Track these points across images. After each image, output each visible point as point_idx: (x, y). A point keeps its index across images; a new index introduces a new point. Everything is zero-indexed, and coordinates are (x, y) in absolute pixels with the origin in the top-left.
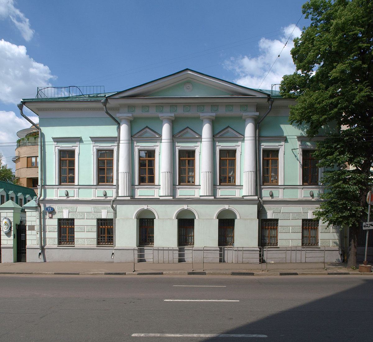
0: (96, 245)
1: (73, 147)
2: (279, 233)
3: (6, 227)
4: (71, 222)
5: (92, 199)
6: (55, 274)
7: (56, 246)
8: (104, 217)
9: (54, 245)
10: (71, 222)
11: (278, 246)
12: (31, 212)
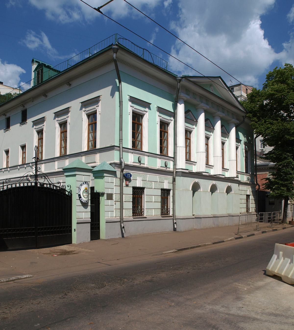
0: (160, 216)
1: (170, 120)
2: (125, 202)
3: (86, 195)
4: (142, 189)
5: (158, 169)
6: (214, 243)
7: (131, 218)
8: (138, 185)
9: (130, 216)
10: (142, 189)
11: (145, 216)
12: (110, 177)
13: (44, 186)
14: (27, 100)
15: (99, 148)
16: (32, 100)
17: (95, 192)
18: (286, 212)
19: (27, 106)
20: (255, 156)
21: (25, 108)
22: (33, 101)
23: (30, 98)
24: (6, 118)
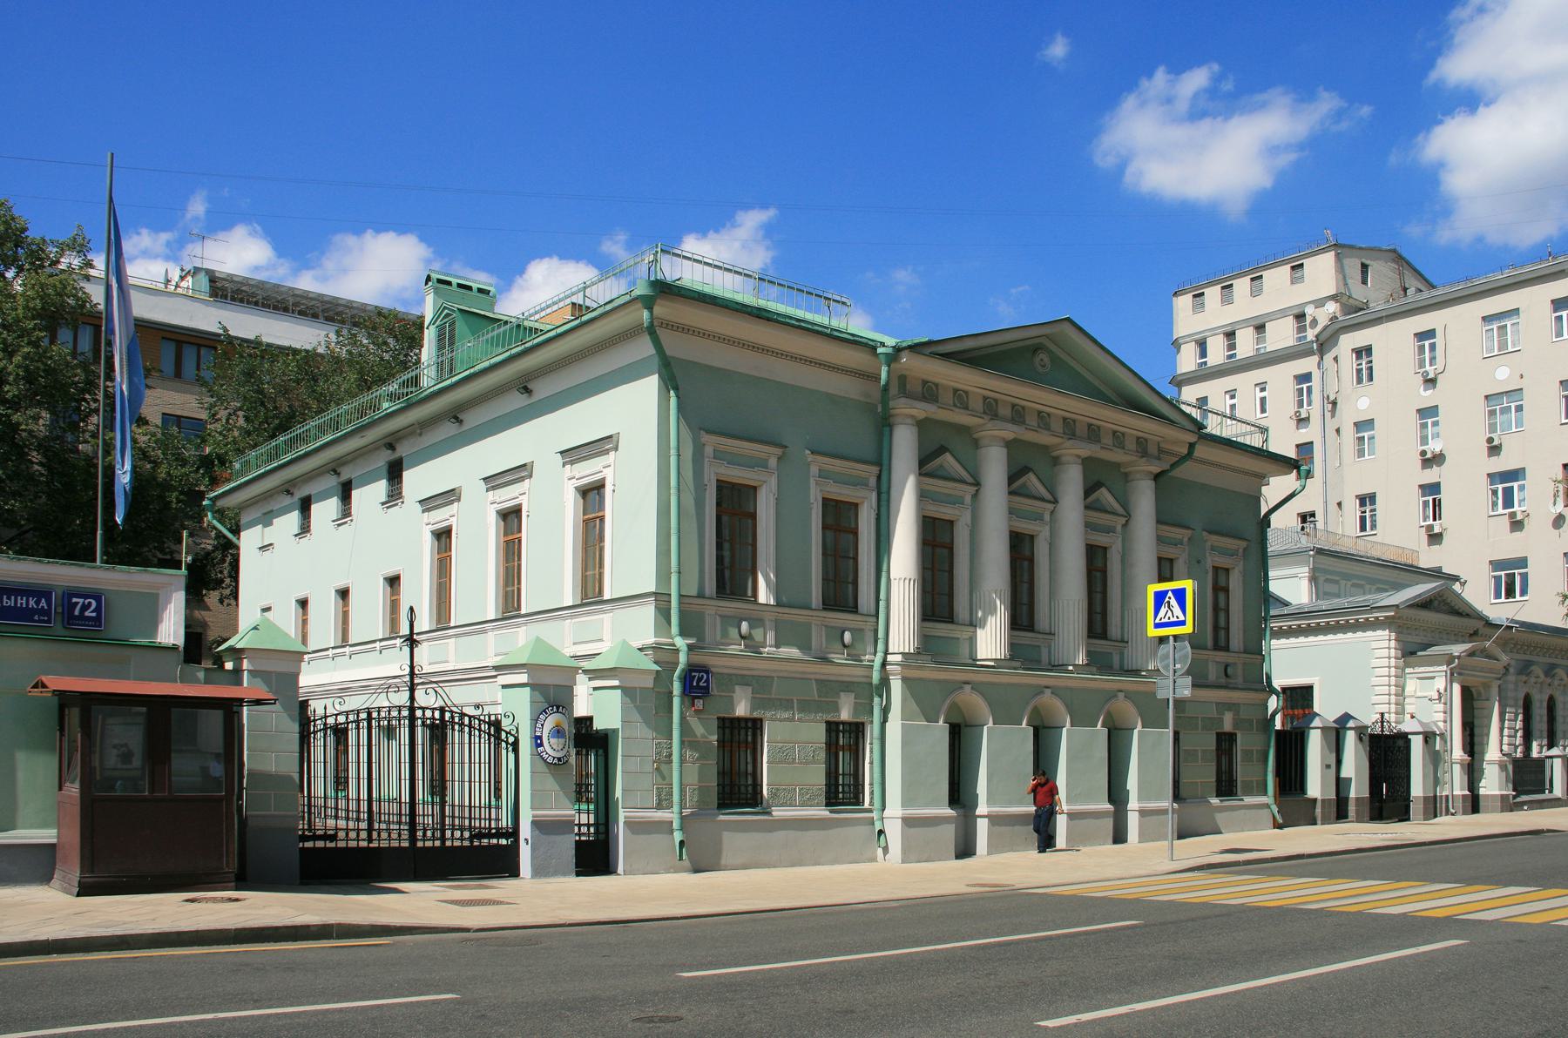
13: (176, 591)
14: (400, 430)
15: (609, 598)
16: (418, 431)
17: (595, 729)
18: (1241, 809)
19: (403, 450)
20: (245, 786)
21: (396, 455)
22: (420, 435)
23: (413, 424)
24: (339, 483)
